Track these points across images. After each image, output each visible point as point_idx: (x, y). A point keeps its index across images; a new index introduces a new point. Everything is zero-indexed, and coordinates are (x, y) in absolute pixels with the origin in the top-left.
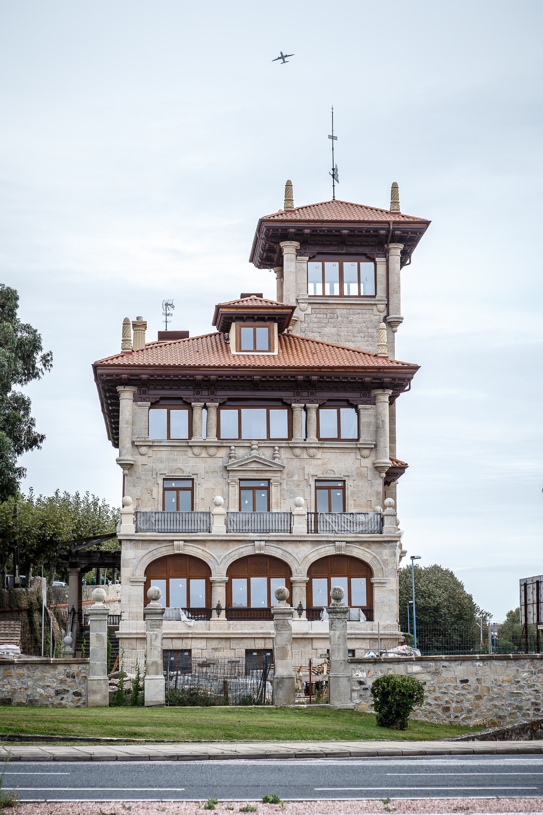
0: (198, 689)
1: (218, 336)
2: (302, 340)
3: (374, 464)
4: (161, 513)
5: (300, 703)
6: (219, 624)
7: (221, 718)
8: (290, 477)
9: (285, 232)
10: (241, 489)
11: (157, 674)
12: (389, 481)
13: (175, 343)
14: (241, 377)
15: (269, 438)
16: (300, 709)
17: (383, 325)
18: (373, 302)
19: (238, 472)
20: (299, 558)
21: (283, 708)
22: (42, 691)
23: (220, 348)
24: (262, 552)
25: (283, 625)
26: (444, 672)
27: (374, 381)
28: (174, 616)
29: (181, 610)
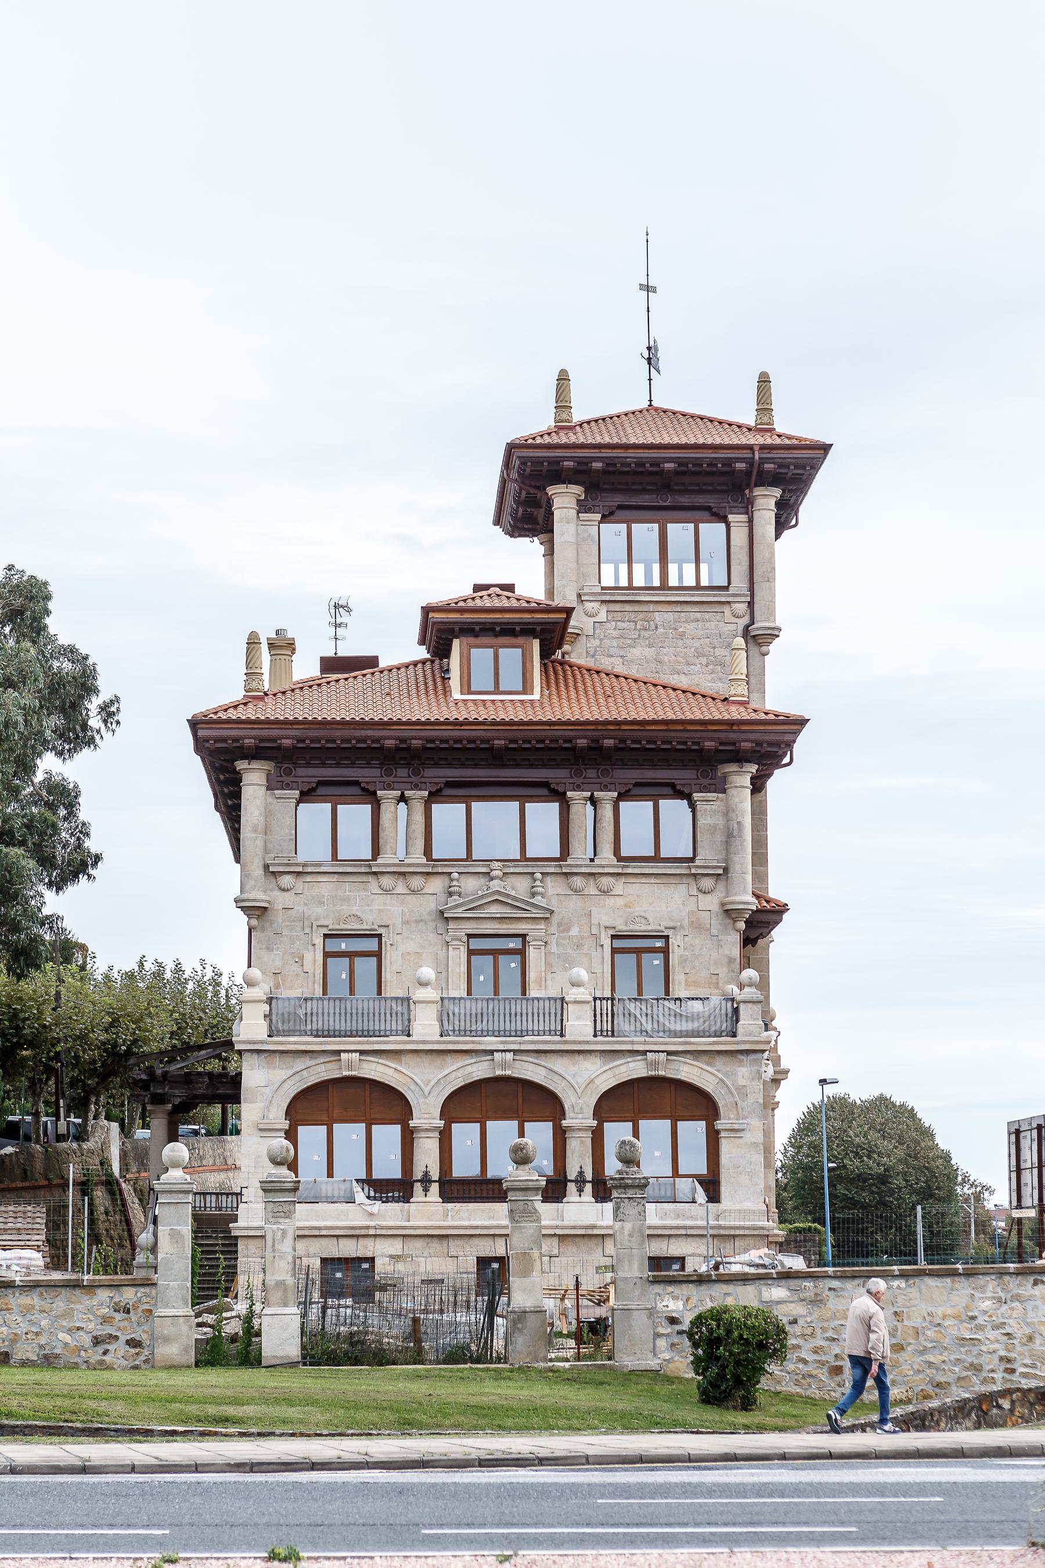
0: (367, 1333)
1: (428, 665)
2: (589, 670)
3: (723, 904)
4: (318, 999)
5: (558, 1359)
6: (427, 1210)
7: (395, 1389)
8: (564, 931)
9: (555, 467)
10: (471, 953)
11: (285, 1305)
12: (752, 937)
13: (346, 679)
14: (469, 742)
15: (524, 857)
16: (558, 1371)
17: (740, 642)
18: (723, 599)
19: (464, 921)
20: (577, 1083)
21: (524, 1370)
22: (67, 1338)
23: (431, 687)
24: (508, 1073)
25: (524, 1211)
26: (831, 1299)
27: (721, 748)
28: (342, 1193)
29: (354, 1182)
